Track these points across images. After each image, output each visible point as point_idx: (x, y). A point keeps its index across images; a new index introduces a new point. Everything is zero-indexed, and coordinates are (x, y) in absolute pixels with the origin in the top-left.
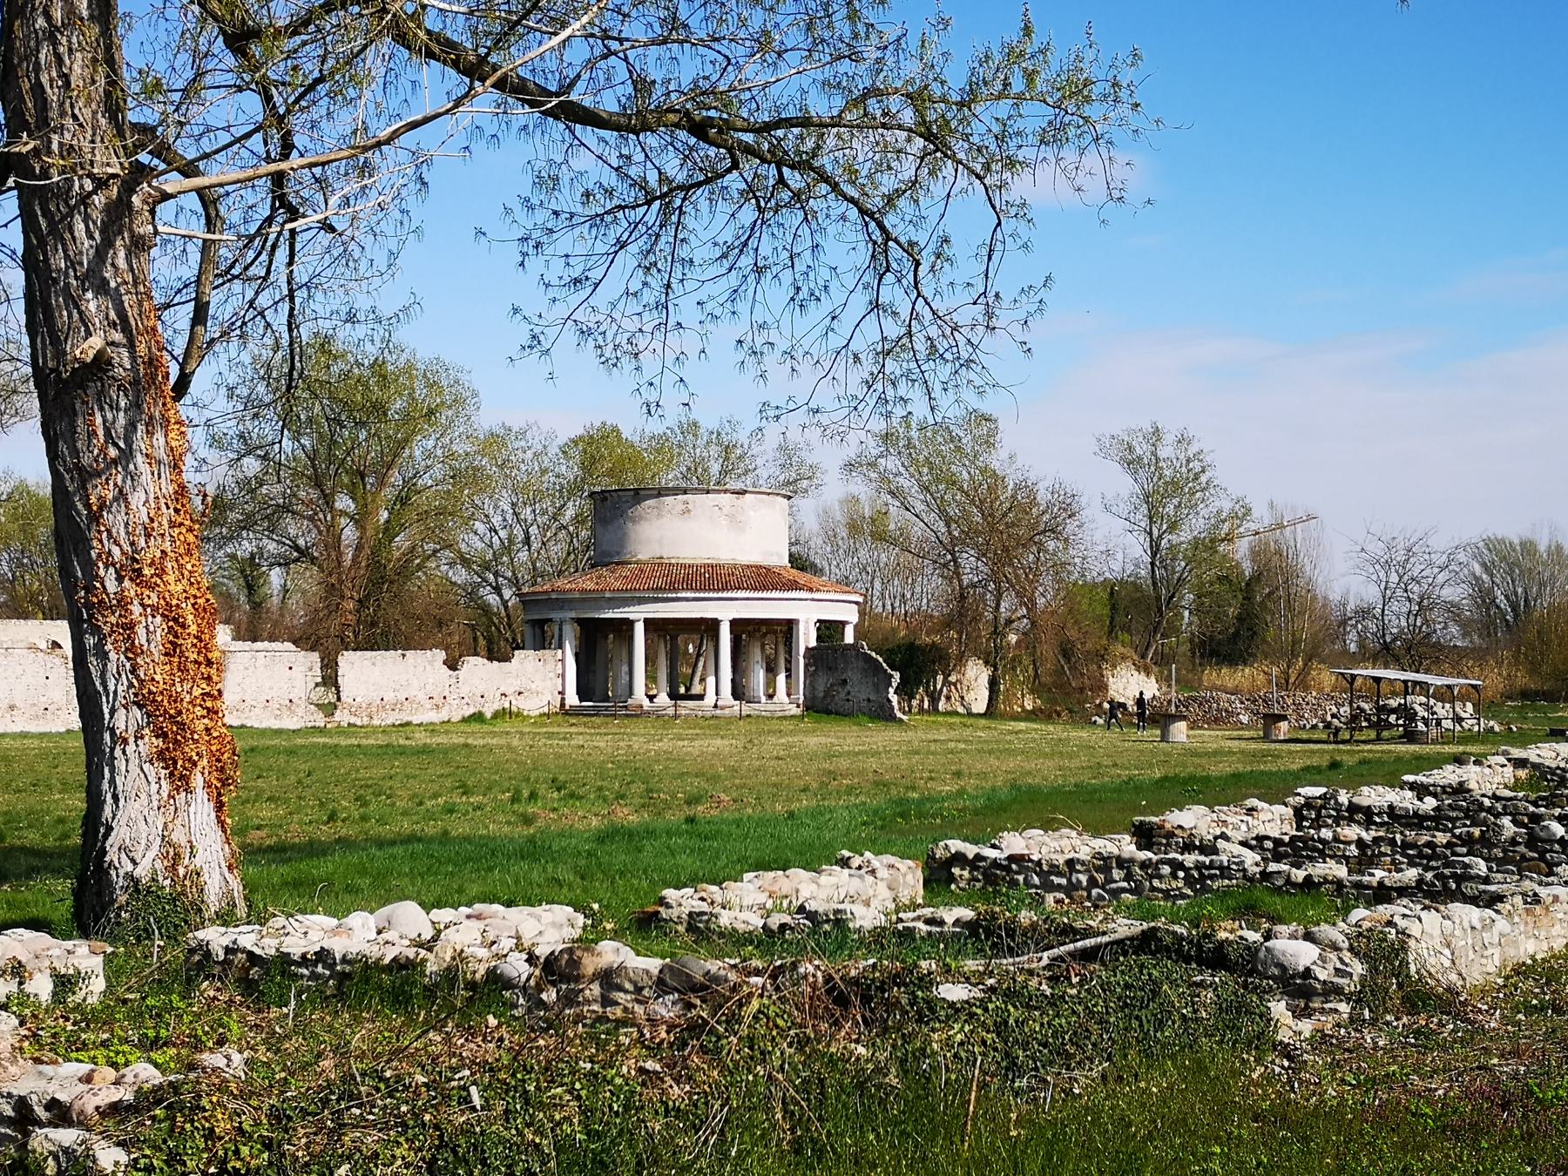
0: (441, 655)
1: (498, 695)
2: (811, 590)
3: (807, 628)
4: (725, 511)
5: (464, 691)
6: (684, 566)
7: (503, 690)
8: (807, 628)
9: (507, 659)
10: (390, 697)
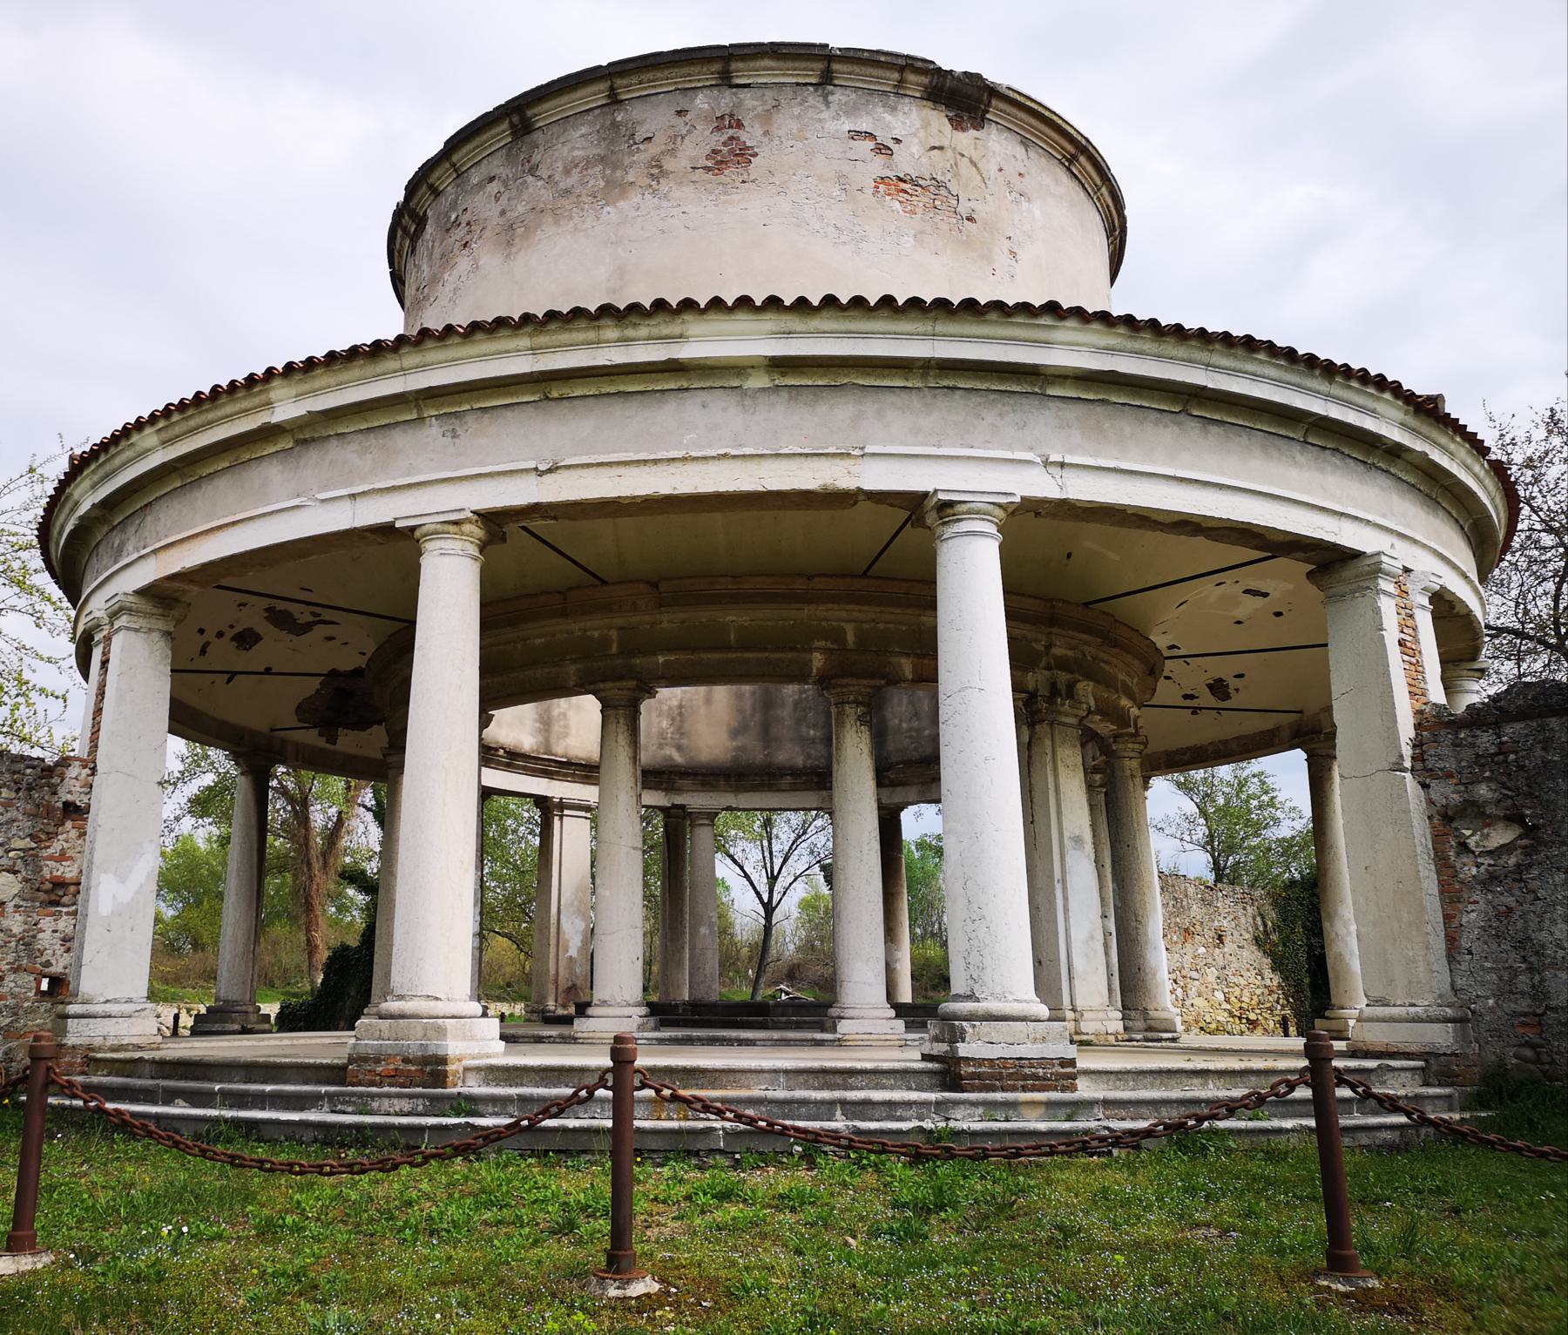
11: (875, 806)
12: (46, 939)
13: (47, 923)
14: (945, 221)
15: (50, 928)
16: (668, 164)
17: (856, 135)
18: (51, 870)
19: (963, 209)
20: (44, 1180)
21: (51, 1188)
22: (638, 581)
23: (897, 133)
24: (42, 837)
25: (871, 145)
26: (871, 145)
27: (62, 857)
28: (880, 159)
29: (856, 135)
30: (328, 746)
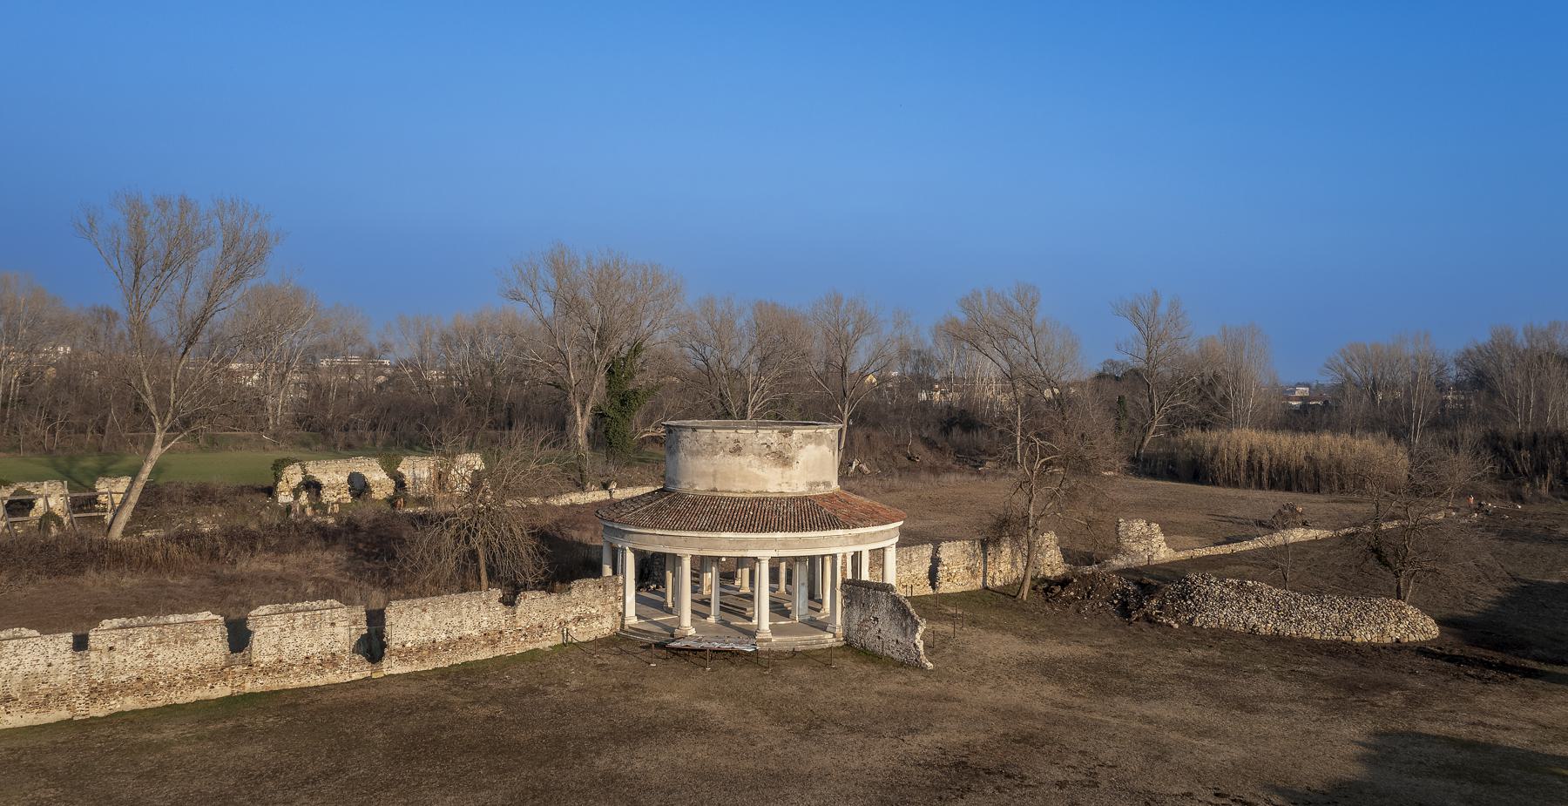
3: (844, 562)
5: (522, 623)
8: (844, 562)
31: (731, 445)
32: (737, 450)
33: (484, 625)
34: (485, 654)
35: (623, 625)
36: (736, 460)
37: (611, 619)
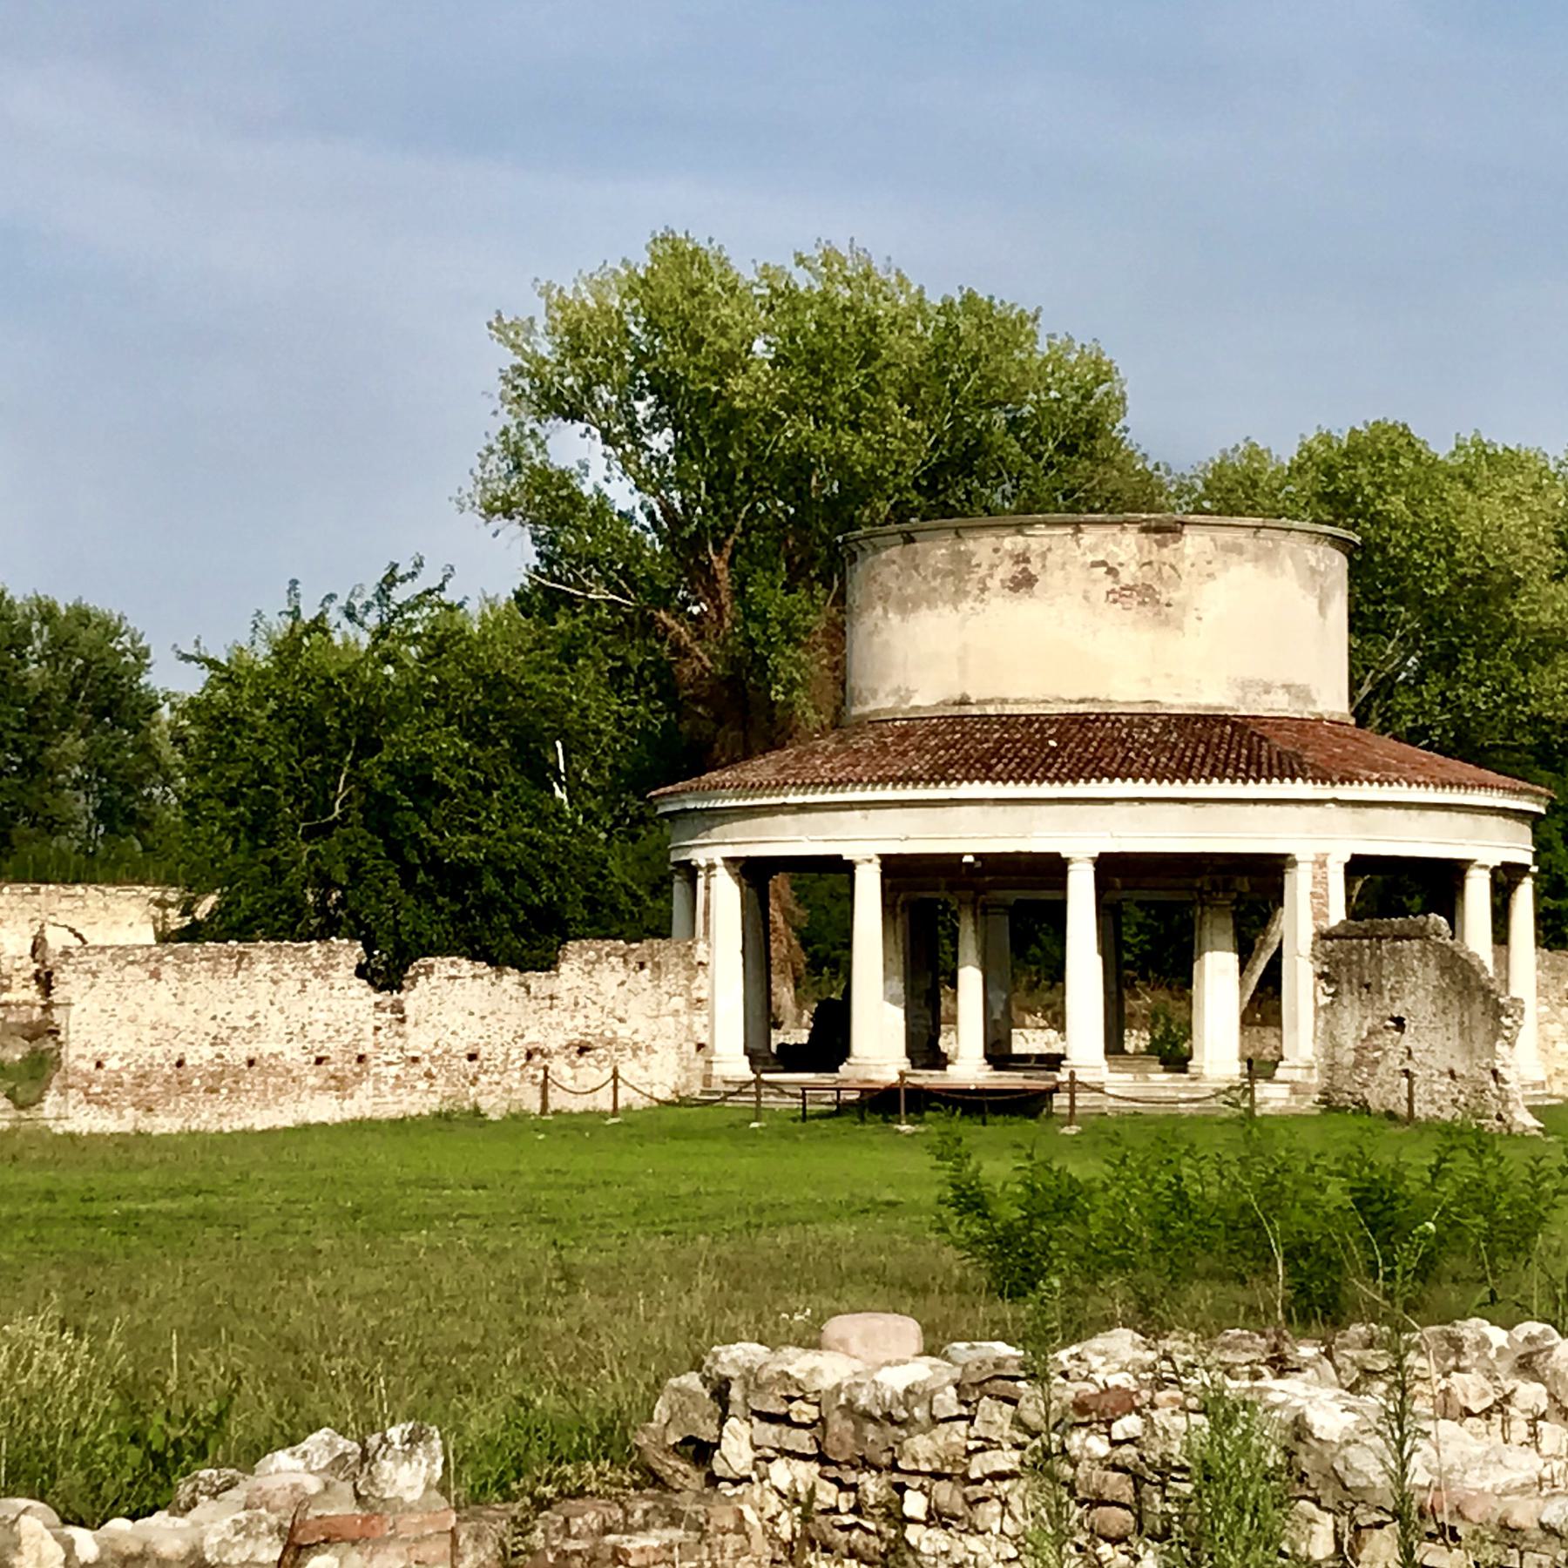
0: (349, 953)
1: (517, 1053)
2: (1324, 778)
3: (1321, 881)
4: (1126, 578)
5: (419, 1040)
6: (1007, 721)
7: (533, 1037)
8: (1321, 881)
9: (548, 964)
10: (200, 1055)
11: (1345, 598)
12: (697, 1027)
13: (696, 1019)
14: (1148, 611)
15: (699, 1020)
16: (989, 583)
17: (1095, 565)
18: (696, 994)
19: (1163, 600)
20: (1127, 1011)
21: (1132, 1015)
22: (999, 906)
23: (1121, 560)
24: (690, 979)
25: (1104, 569)
26: (1104, 569)
27: (700, 988)
28: (1110, 578)
29: (1095, 565)
30: (1161, 1082)
31: (1007, 570)
32: (1024, 582)
33: (317, 1033)
34: (325, 1109)
35: (707, 1079)
36: (1025, 609)
37: (673, 1058)
